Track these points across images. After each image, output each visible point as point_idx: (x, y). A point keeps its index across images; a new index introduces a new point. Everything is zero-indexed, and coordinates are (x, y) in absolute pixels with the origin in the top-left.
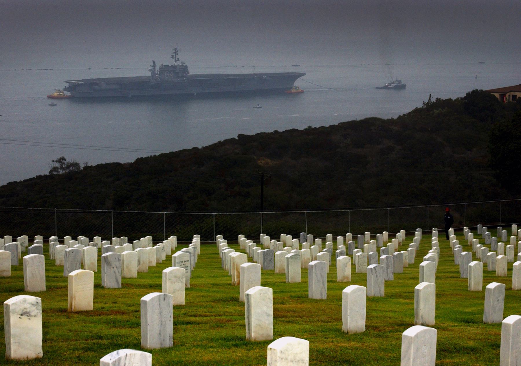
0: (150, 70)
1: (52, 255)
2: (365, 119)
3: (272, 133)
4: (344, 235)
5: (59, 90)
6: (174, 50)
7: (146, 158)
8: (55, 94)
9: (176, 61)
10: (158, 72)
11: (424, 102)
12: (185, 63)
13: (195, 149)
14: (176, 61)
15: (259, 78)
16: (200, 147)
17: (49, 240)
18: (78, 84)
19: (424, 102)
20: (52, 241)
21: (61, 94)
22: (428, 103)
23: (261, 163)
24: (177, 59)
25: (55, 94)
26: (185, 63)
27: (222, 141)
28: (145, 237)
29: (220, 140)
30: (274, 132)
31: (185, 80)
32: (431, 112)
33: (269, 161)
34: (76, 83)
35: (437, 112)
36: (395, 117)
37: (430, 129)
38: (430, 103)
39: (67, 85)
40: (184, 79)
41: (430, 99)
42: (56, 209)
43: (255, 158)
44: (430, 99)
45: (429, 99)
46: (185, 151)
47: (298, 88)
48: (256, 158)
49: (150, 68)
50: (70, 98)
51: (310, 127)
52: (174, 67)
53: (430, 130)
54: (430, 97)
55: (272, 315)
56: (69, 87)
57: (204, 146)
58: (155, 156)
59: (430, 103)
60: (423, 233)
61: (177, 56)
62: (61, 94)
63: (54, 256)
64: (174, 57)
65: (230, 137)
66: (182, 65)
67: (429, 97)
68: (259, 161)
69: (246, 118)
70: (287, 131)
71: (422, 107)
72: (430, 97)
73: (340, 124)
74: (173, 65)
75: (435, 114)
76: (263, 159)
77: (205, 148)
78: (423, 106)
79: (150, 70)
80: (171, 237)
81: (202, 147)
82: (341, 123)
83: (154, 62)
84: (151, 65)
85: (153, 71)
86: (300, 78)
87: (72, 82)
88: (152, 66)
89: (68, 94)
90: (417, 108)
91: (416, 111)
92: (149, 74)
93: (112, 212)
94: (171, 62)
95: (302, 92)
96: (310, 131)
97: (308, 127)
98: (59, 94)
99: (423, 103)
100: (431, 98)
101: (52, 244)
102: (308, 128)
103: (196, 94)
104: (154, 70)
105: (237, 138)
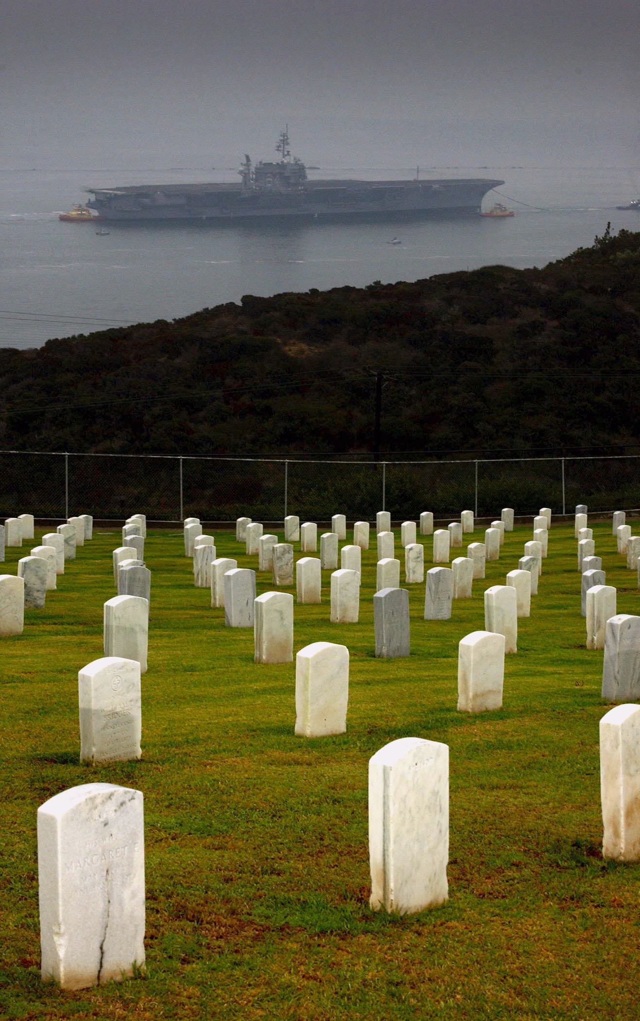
0: (241, 172)
1: (200, 578)
2: (481, 269)
3: (307, 293)
4: (416, 518)
5: (80, 206)
6: (281, 136)
7: (65, 341)
8: (74, 213)
9: (284, 156)
10: (254, 176)
11: (597, 236)
12: (299, 160)
13: (161, 323)
14: (284, 156)
15: (425, 189)
16: (170, 320)
17: (123, 532)
18: (116, 195)
19: (597, 236)
20: (128, 532)
21: (83, 212)
22: (605, 239)
23: (290, 350)
24: (286, 153)
25: (74, 213)
26: (299, 160)
27: (210, 309)
28: (77, 516)
29: (206, 307)
30: (309, 292)
31: (300, 190)
32: (612, 257)
33: (304, 346)
34: (111, 194)
35: (624, 256)
36: (541, 266)
37: (609, 289)
38: (607, 240)
39: (93, 198)
40: (300, 188)
41: (608, 232)
42: (66, 453)
43: (279, 340)
44: (608, 232)
45: (606, 231)
46: (140, 326)
47: (505, 208)
48: (280, 342)
49: (241, 168)
50: (96, 221)
51: (378, 283)
52: (282, 166)
53: (611, 291)
54: (609, 227)
55: (440, 746)
56: (97, 200)
57: (177, 318)
58: (81, 336)
59: (609, 240)
60: (554, 520)
61: (286, 146)
62: (83, 212)
63: (205, 579)
64: (282, 149)
65: (224, 301)
66: (296, 164)
67: (606, 228)
68: (287, 348)
69: (225, 262)
70: (335, 290)
71: (594, 246)
72: (609, 227)
73: (433, 279)
74: (280, 163)
75: (618, 261)
76: (294, 344)
77: (180, 322)
78: (595, 244)
79: (241, 172)
80: (134, 517)
81: (173, 320)
82: (436, 276)
83: (248, 158)
84: (242, 164)
85: (245, 175)
86: (494, 189)
87: (103, 193)
88: (244, 165)
89: (95, 213)
90: (581, 248)
91: (582, 255)
92: (239, 179)
93: (181, 460)
94: (275, 158)
95: (511, 215)
96: (376, 290)
97: (375, 283)
98: (80, 213)
99: (596, 240)
100: (611, 229)
101: (201, 549)
102: (373, 285)
103: (316, 216)
104: (247, 172)
105: (240, 304)
